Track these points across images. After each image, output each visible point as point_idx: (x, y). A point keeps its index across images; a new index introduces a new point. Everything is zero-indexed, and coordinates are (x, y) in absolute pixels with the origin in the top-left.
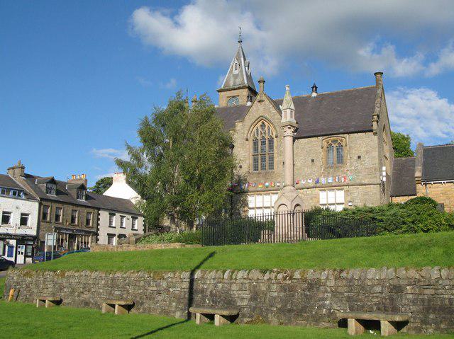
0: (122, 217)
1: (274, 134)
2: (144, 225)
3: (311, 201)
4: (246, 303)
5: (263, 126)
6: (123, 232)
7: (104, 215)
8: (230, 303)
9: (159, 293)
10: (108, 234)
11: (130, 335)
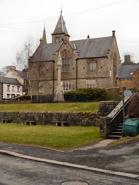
0: (92, 69)
1: (70, 57)
2: (3, 94)
3: (83, 84)
4: (38, 119)
5: (66, 53)
6: (13, 93)
7: (5, 86)
8: (34, 119)
9: (17, 117)
10: (7, 94)
11: (131, 120)
